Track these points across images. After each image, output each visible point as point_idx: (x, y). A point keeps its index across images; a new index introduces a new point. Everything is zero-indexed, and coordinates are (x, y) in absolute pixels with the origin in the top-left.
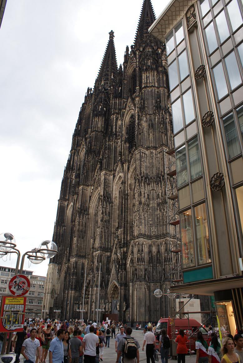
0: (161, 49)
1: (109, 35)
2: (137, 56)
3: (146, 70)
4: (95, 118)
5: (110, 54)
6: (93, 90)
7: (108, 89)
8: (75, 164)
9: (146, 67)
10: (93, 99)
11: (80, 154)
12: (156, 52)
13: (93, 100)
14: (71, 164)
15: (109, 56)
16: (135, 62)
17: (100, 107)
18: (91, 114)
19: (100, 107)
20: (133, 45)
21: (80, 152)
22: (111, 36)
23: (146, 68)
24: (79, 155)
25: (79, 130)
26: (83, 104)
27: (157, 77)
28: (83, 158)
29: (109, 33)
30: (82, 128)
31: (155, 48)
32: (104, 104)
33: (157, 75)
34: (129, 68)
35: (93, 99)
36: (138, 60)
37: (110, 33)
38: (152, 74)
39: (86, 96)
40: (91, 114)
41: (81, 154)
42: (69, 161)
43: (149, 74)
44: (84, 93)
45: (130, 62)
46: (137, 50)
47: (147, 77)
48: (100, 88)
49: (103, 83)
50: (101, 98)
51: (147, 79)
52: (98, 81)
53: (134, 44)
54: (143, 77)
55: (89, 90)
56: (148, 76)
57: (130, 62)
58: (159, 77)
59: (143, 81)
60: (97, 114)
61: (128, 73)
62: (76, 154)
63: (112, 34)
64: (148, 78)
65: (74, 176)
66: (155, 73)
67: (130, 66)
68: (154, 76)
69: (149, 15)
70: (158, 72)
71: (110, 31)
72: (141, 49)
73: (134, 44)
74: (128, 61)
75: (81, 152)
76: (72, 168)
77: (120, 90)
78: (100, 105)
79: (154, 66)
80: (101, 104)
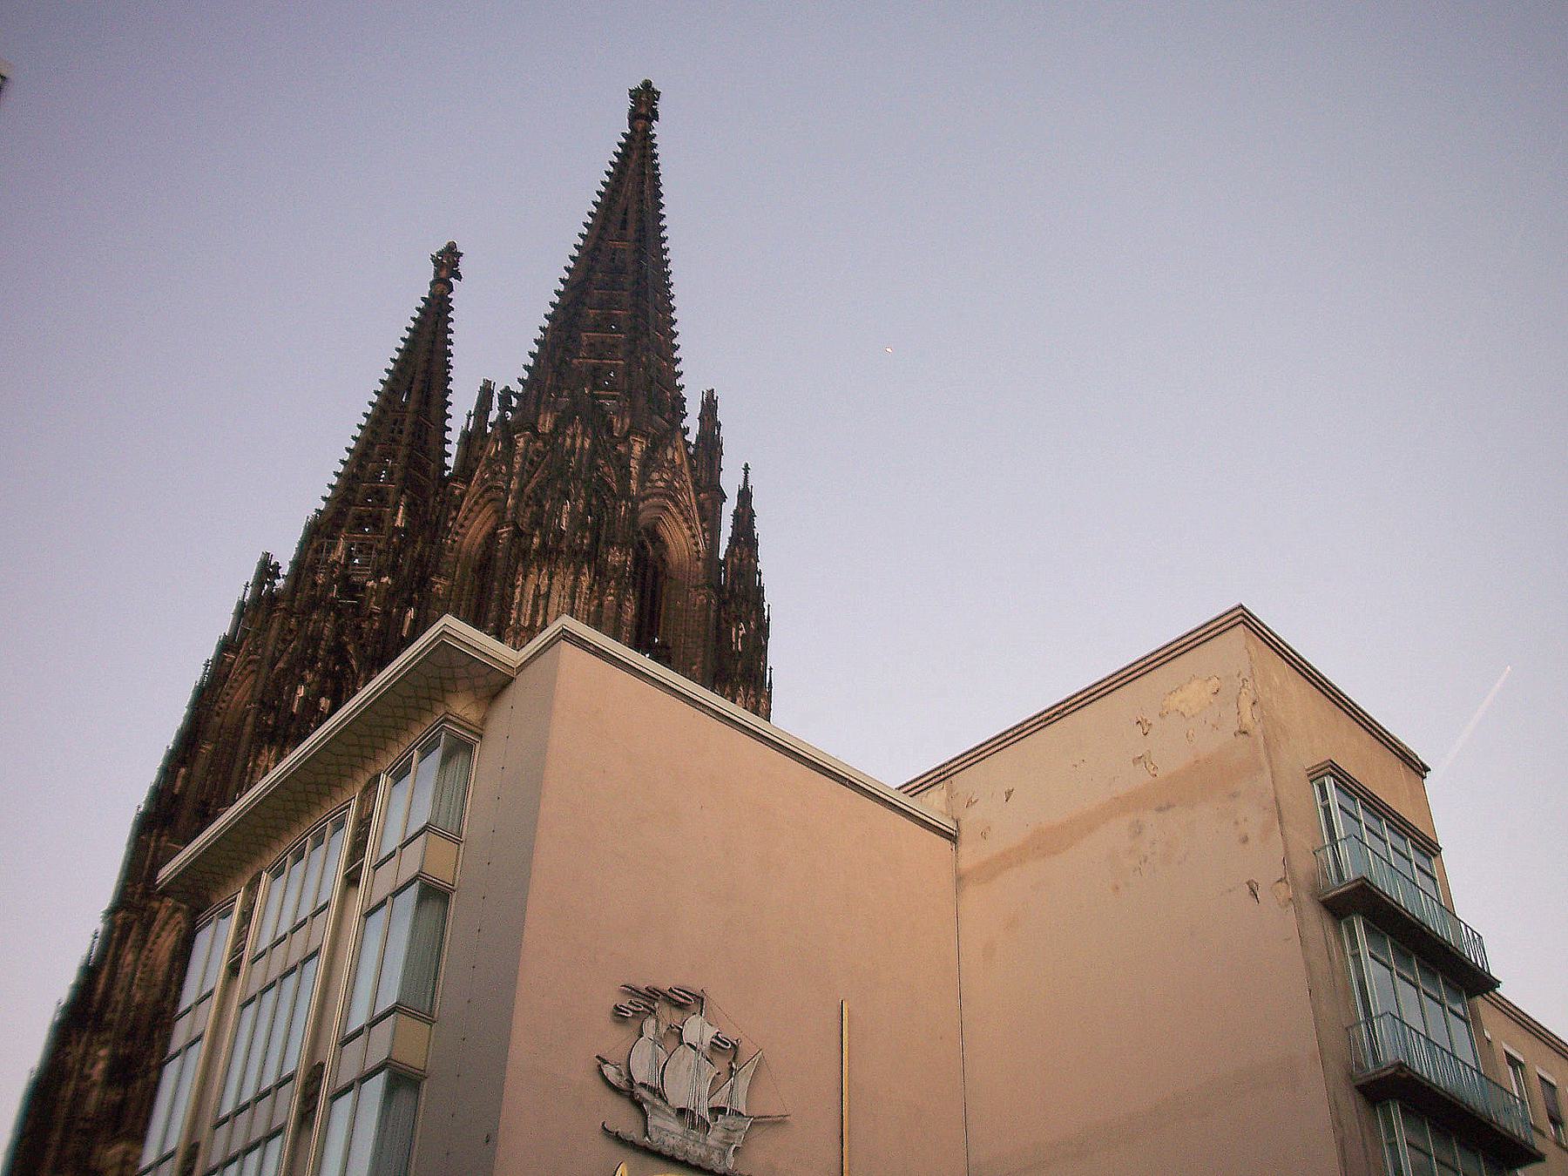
0: (645, 435)
1: (627, 104)
2: (518, 459)
3: (548, 555)
4: (259, 753)
5: (419, 377)
6: (284, 571)
7: (364, 588)
8: (119, 996)
9: (543, 536)
10: (273, 633)
11: (154, 943)
12: (622, 449)
13: (271, 641)
14: (94, 989)
15: (625, 221)
16: (501, 488)
17: (301, 692)
18: (250, 719)
19: (301, 692)
20: (516, 395)
21: (156, 927)
22: (443, 274)
23: (544, 544)
24: (149, 944)
25: (175, 798)
26: (226, 645)
27: (588, 602)
28: (165, 967)
29: (435, 261)
30: (193, 786)
31: (617, 423)
32: (327, 674)
33: (590, 588)
34: (470, 510)
35: (273, 633)
36: (514, 485)
37: (635, 95)
38: (569, 583)
39: (242, 604)
40: (250, 719)
41: (160, 940)
42: (90, 973)
43: (550, 579)
44: (237, 585)
45: (484, 481)
46: (520, 428)
47: (537, 596)
48: (320, 579)
49: (339, 553)
50: (314, 640)
51: (535, 605)
52: (319, 532)
53: (519, 389)
54: (518, 590)
55: (267, 569)
56: (543, 589)
57: (484, 481)
58: (601, 605)
59: (514, 615)
60: (276, 727)
61: (464, 536)
62: (133, 935)
63: (448, 263)
64: (542, 603)
65: (101, 1066)
66: (585, 581)
67: (476, 503)
68: (573, 598)
69: (631, 232)
70: (600, 573)
71: (637, 84)
72: (546, 424)
73: (519, 389)
74: (473, 472)
75: (162, 929)
76: (99, 1016)
77: (408, 623)
78: (302, 680)
79: (582, 537)
80: (309, 677)
